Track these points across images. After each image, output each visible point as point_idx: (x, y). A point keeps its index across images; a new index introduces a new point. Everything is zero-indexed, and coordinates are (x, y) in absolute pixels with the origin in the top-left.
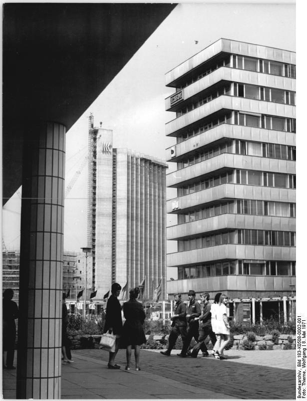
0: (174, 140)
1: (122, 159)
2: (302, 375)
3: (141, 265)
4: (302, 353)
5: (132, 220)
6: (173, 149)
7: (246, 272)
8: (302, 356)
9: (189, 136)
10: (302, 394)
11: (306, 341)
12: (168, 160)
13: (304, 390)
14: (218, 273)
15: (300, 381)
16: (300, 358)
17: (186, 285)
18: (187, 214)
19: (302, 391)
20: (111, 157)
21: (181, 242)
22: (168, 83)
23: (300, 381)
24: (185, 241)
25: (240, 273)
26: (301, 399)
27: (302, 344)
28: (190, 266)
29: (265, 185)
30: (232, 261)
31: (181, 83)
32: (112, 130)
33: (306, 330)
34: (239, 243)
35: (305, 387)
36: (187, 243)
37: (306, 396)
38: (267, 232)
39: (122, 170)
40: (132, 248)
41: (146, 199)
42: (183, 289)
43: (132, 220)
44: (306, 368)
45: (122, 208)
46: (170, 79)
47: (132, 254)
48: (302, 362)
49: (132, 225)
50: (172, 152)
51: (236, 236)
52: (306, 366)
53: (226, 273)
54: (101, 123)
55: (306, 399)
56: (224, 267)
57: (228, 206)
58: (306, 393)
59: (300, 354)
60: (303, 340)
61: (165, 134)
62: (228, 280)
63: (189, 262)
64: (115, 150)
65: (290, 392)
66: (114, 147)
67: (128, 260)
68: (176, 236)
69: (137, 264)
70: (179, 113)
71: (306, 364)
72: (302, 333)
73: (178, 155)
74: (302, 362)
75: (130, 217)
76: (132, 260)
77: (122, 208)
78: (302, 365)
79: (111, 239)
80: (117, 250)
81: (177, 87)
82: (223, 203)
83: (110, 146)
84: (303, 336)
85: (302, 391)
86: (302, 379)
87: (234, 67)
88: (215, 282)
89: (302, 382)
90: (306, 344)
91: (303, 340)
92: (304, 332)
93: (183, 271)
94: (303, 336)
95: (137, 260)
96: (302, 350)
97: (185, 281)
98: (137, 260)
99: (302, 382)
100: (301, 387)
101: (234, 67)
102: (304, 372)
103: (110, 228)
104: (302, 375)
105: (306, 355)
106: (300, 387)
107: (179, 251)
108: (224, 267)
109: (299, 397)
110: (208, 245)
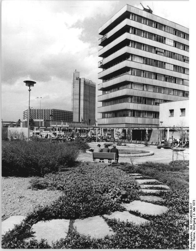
0: (102, 58)
1: (82, 81)
2: (193, 235)
3: (88, 115)
4: (193, 221)
5: (85, 101)
6: (101, 62)
7: (134, 116)
8: (193, 223)
9: (109, 79)
10: (193, 247)
11: (195, 214)
12: (99, 100)
13: (194, 244)
14: (121, 116)
15: (192, 239)
16: (191, 224)
17: (106, 121)
18: (107, 91)
19: (193, 245)
20: (79, 81)
21: (104, 103)
22: (99, 33)
23: (192, 239)
24: (106, 102)
25: (131, 116)
26: (192, 250)
27: (193, 215)
28: (107, 113)
29: (143, 77)
30: (126, 110)
31: (104, 33)
32: (79, 72)
33: (195, 206)
34: (131, 102)
35: (195, 242)
36: (106, 103)
37: (195, 248)
38: (143, 97)
39: (82, 86)
40: (85, 110)
41: (90, 94)
42: (104, 122)
43: (85, 101)
44: (195, 230)
45: (82, 97)
46: (100, 30)
47: (85, 111)
48: (193, 227)
49: (85, 102)
50: (101, 63)
51: (130, 99)
52: (195, 229)
53: (124, 116)
54: (76, 70)
55: (195, 250)
56: (123, 113)
57: (126, 99)
58: (195, 246)
59: (192, 222)
60: (193, 213)
61: (98, 78)
62: (126, 119)
63: (107, 111)
64: (80, 79)
65: (184, 242)
66: (80, 78)
67: (84, 114)
68: (101, 100)
69: (86, 115)
70: (104, 80)
71: (195, 228)
72: (193, 209)
73: (103, 64)
74: (193, 227)
75: (85, 100)
76: (85, 113)
77: (82, 97)
78: (193, 228)
79: (78, 107)
80: (81, 110)
81: (103, 68)
82: (124, 98)
83: (79, 78)
84: (193, 210)
85: (193, 245)
86: (193, 237)
87: (132, 46)
88: (120, 119)
89: (193, 239)
90: (195, 215)
91: (193, 213)
92: (194, 208)
93: (104, 114)
94: (193, 210)
95: (86, 113)
96: (193, 219)
97: (105, 119)
98: (86, 113)
99: (193, 239)
100: (192, 242)
101: (132, 46)
102: (194, 233)
103: (78, 104)
104: (193, 235)
105: (195, 222)
106: (191, 242)
107: (103, 106)
108: (123, 113)
109: (191, 249)
110: (116, 103)
